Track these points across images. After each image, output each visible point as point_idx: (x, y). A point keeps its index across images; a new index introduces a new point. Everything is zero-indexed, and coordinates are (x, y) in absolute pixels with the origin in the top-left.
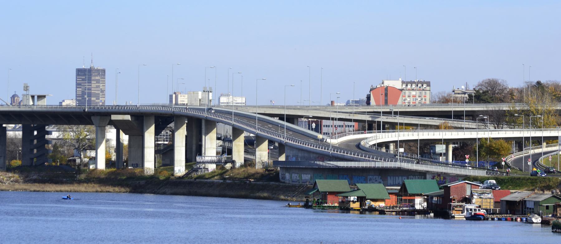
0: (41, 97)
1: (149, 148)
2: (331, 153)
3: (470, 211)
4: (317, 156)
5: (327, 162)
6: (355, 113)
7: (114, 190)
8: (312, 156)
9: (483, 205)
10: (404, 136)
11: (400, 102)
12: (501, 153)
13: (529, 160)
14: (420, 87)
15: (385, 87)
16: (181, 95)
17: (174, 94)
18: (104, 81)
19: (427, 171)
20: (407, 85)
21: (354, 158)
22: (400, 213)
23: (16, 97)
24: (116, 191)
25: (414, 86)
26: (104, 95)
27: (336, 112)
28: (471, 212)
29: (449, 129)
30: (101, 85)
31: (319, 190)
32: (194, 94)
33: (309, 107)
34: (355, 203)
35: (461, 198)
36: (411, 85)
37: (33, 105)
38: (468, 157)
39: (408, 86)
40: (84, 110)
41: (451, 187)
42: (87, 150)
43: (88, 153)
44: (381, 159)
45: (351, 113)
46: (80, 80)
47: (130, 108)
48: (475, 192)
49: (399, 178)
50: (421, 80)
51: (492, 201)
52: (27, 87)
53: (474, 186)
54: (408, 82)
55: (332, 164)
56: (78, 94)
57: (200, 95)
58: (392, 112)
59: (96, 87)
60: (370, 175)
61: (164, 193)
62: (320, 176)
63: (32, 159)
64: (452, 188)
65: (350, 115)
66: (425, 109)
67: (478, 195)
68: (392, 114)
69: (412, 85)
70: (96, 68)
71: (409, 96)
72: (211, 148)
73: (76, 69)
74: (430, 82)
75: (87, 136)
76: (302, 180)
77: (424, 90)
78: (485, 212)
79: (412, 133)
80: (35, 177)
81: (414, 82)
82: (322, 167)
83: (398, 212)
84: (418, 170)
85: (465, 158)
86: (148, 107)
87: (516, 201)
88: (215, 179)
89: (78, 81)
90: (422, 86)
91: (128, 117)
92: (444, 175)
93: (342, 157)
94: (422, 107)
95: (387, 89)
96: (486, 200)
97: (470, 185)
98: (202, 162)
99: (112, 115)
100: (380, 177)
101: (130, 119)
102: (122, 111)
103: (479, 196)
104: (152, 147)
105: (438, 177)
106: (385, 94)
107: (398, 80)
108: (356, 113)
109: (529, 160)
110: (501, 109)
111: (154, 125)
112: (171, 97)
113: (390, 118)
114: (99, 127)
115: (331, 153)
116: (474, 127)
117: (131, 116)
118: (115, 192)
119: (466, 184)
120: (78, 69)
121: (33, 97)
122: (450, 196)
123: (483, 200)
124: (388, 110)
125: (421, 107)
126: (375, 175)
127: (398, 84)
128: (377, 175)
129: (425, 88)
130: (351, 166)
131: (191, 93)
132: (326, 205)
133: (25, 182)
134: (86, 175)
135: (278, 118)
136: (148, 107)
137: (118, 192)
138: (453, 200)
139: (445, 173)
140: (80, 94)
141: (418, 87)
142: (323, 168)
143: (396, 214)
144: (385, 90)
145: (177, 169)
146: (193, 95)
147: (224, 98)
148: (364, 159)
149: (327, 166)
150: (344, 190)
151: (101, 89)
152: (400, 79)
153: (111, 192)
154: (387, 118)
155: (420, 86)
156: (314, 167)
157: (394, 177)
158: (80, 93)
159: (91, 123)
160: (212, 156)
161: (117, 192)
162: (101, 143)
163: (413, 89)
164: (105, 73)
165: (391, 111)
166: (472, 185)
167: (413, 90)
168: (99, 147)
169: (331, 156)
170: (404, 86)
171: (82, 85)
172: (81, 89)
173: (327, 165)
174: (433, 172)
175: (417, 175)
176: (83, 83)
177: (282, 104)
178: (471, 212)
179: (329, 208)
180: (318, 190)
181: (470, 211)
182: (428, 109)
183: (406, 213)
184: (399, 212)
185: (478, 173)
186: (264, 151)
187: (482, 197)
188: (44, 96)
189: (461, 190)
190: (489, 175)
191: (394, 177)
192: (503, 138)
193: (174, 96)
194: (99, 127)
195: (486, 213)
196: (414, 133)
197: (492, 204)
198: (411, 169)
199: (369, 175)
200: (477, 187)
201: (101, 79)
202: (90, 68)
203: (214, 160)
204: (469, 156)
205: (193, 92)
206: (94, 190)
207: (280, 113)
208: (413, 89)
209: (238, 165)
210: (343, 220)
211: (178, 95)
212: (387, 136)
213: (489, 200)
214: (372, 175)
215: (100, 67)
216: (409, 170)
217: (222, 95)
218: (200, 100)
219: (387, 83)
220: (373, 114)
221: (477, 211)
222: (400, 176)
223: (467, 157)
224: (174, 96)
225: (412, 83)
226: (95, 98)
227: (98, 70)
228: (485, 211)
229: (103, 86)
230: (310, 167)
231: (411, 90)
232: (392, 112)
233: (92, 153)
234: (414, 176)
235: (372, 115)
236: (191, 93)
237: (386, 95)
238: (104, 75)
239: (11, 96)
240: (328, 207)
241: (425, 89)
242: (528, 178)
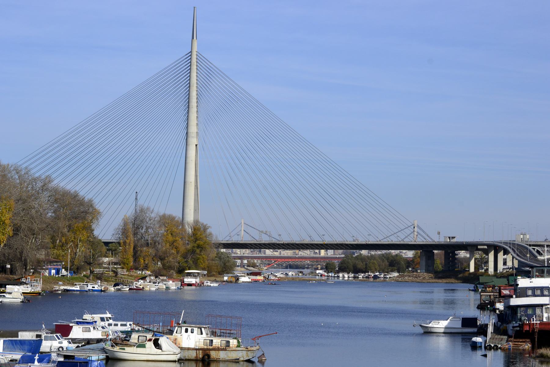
0: (453, 238)
7: (455, 282)
37: (450, 241)
40: (463, 244)
52: (439, 232)
57: (522, 236)
63: (449, 267)
80: (440, 276)
91: (486, 247)
118: (455, 283)
121: (449, 238)
133: (435, 278)
135: (63, 238)
145: (471, 270)
161: (456, 283)
162: (472, 259)
188: (455, 237)
194: (471, 251)
206: (446, 282)
210: (530, 292)
218: (522, 239)
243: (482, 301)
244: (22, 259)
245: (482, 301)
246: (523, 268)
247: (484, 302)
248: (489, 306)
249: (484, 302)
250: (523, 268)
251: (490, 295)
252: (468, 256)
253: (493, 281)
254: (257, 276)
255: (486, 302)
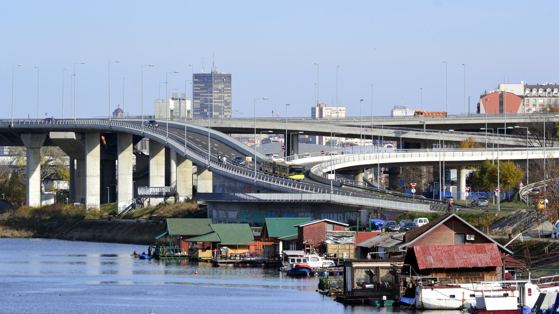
1: (93, 176)
2: (255, 181)
3: (291, 262)
4: (244, 186)
5: (248, 194)
6: (374, 128)
7: (12, 234)
8: (238, 185)
9: (339, 253)
10: (370, 159)
11: (520, 111)
12: (509, 181)
13: (497, 189)
14: (549, 93)
15: (500, 93)
16: (327, 108)
17: (318, 106)
18: (231, 90)
19: (361, 206)
20: (531, 91)
21: (281, 188)
22: (240, 265)
23: (119, 112)
24: (16, 235)
25: (541, 91)
26: (230, 108)
27: (359, 126)
28: (292, 263)
29: (476, 148)
30: (226, 95)
31: (170, 234)
32: (163, 102)
33: (192, 120)
34: (205, 251)
35: (318, 243)
36: (537, 90)
38: (415, 186)
39: (533, 91)
40: (10, 126)
41: (304, 228)
42: (54, 180)
43: (55, 185)
44: (311, 190)
45: (370, 127)
46: (198, 88)
47: (65, 122)
48: (331, 234)
49: (333, 215)
50: (551, 83)
51: (353, 247)
53: (338, 226)
54: (534, 85)
55: (254, 197)
56: (196, 107)
57: (172, 105)
58: (423, 125)
59: (219, 98)
60: (302, 212)
61: (71, 239)
62: (247, 214)
64: (306, 229)
65: (366, 130)
66: (470, 120)
67: (334, 239)
68: (423, 128)
69: (538, 90)
70: (219, 73)
71: (535, 105)
72: (157, 175)
73: (231, 74)
74: (196, 76)
75: (49, 161)
76: (228, 218)
77: (554, 97)
78: (332, 264)
79: (403, 153)
81: (541, 86)
82: (242, 201)
83: (237, 263)
84: (350, 204)
85: (411, 188)
86: (83, 121)
87: (367, 248)
88: (144, 219)
89: (196, 90)
90: (553, 91)
91: (72, 135)
92: (382, 212)
93: (268, 186)
94: (470, 118)
95: (501, 96)
96: (344, 245)
97: (331, 226)
98: (152, 195)
99: (50, 133)
100: (312, 214)
101: (75, 138)
102: (61, 126)
103: (335, 241)
104: (97, 176)
105: (374, 215)
106: (500, 102)
107: (520, 83)
108: (375, 127)
109: (497, 189)
110: (551, 120)
111: (99, 145)
112: (313, 110)
113: (420, 134)
114: (30, 148)
115: (255, 181)
116: (511, 143)
117: (75, 133)
118: (13, 237)
119: (326, 223)
120: (195, 74)
122: (303, 241)
123: (340, 246)
124: (417, 123)
125: (468, 118)
126: (307, 212)
127: (518, 89)
128: (309, 212)
129: (556, 94)
130: (270, 199)
131: (159, 101)
132: (180, 253)
134: (10, 214)
136: (88, 121)
137: (18, 237)
138: (307, 247)
139: (382, 208)
140: (198, 107)
141: (547, 93)
142: (243, 203)
143: (234, 266)
144: (500, 97)
146: (162, 104)
147: (399, 111)
148: (292, 190)
149: (248, 200)
150: (196, 234)
151: (226, 101)
152: (522, 82)
153: (9, 237)
154: (417, 134)
155: (549, 91)
156: (234, 201)
157: (329, 215)
158: (198, 106)
159: (21, 144)
160: (156, 188)
161: (16, 237)
163: (539, 96)
164: (231, 80)
165: (422, 124)
166: (335, 225)
167: (540, 96)
168: (31, 176)
169: (255, 184)
170: (528, 91)
171: (201, 96)
172: (199, 101)
173: (248, 198)
174: (369, 206)
175: (355, 212)
176: (201, 93)
177: (252, 116)
178: (292, 263)
179: (183, 258)
180: (168, 234)
181: (291, 262)
182: (519, 120)
183: (248, 265)
184: (238, 263)
185: (421, 208)
186: (207, 179)
187: (339, 241)
189: (318, 233)
190: (435, 210)
191: (329, 215)
192: (511, 160)
193: (317, 109)
195: (334, 265)
196: (406, 153)
197: (352, 251)
198: (342, 203)
199: (300, 212)
200: (343, 227)
201: (226, 87)
202: (212, 72)
203: (154, 192)
204: (415, 184)
205: (163, 100)
207: (241, 127)
208: (539, 96)
209: (182, 199)
211: (322, 108)
212: (357, 159)
213: (347, 247)
214: (303, 212)
215: (224, 72)
216: (340, 204)
217: (395, 108)
218: (172, 111)
219: (505, 88)
220: (397, 128)
221: (302, 262)
222: (335, 213)
223: (413, 186)
224: (317, 109)
225: (538, 87)
226: (218, 113)
227: (221, 76)
228: (333, 262)
229: (228, 96)
230: (230, 201)
231: (538, 97)
232: (423, 125)
233: (60, 184)
234: (351, 213)
235: (398, 129)
236: (159, 101)
237: (501, 103)
238: (230, 82)
239: (114, 111)
240: (181, 256)
241: (556, 95)
242: (470, 214)
243: (356, 285)
244: (372, 273)
245: (356, 285)
246: (241, 195)
247: (360, 288)
248: (385, 298)
249: (360, 288)
250: (241, 195)
251: (378, 267)
252: (23, 161)
253: (213, 232)
254: (460, 268)
255: (367, 286)
